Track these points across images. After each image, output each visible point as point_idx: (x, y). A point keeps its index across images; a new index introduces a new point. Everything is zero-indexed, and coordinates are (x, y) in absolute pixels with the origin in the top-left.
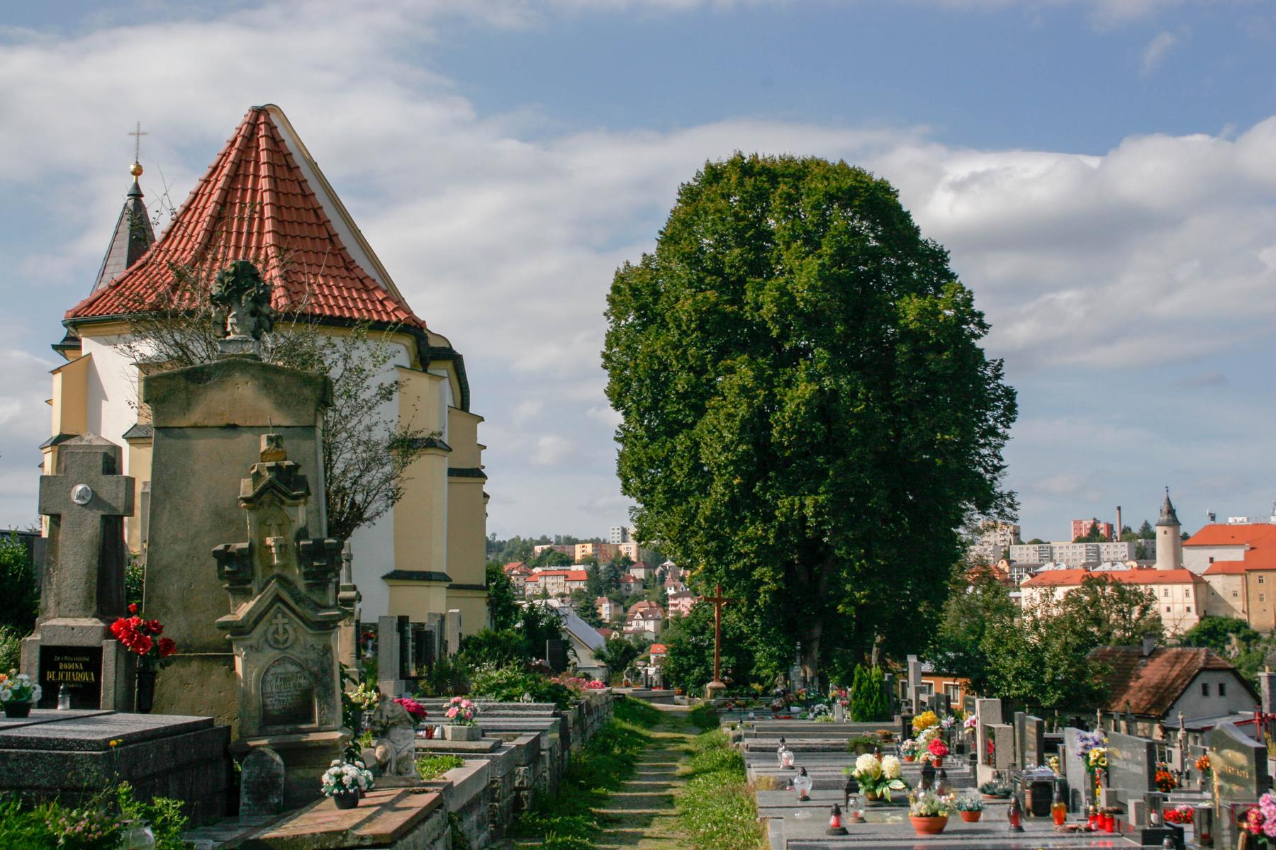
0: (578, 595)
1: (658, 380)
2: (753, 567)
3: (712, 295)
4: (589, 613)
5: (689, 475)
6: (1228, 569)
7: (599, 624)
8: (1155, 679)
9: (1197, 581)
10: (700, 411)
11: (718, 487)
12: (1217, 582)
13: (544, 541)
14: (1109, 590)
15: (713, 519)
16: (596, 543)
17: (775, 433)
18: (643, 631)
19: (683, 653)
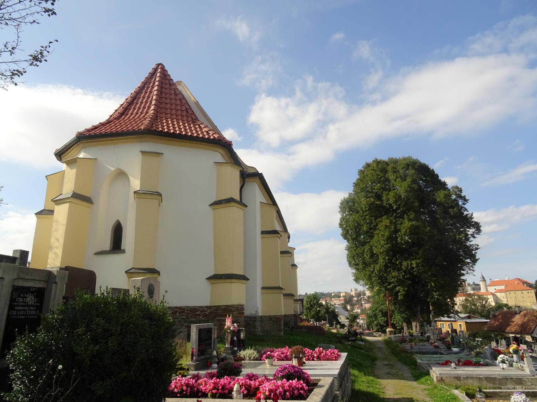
0: (342, 304)
1: (357, 228)
2: (396, 286)
3: (372, 199)
4: (345, 308)
5: (370, 258)
6: (501, 291)
7: (347, 311)
8: (520, 322)
9: (493, 294)
10: (372, 237)
11: (381, 260)
12: (498, 295)
13: (334, 293)
14: (476, 297)
15: (380, 271)
16: (345, 293)
17: (399, 240)
18: (357, 312)
19: (371, 317)
